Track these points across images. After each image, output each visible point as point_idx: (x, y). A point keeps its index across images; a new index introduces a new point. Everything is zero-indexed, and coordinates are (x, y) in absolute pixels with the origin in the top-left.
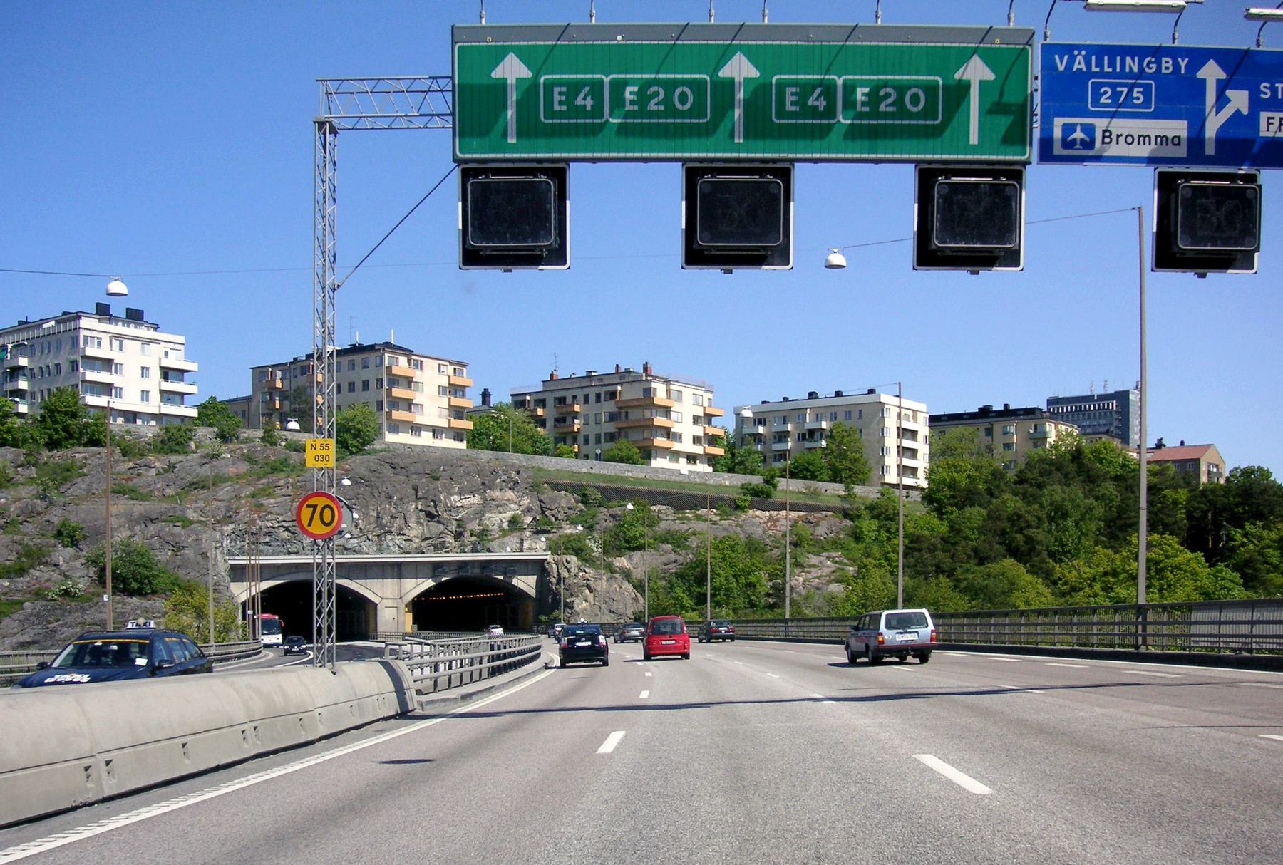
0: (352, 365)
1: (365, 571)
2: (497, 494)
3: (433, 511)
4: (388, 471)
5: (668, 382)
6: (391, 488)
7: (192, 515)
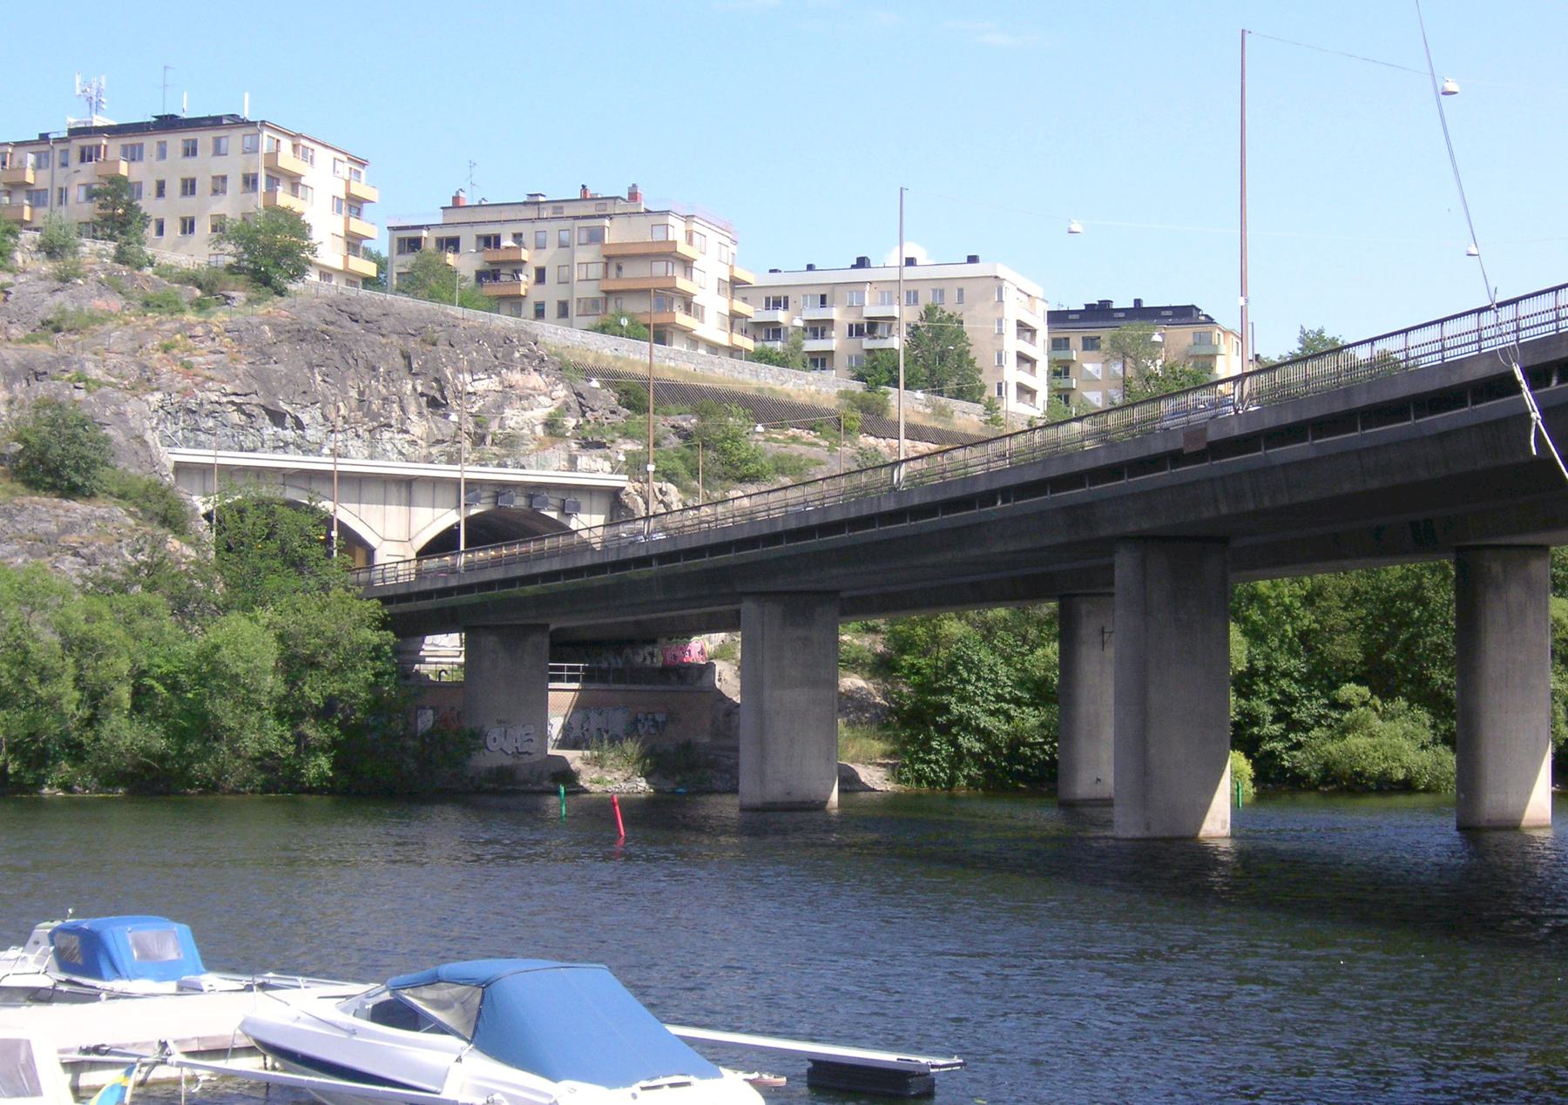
0: (191, 150)
1: (358, 484)
2: (515, 377)
3: (438, 396)
5: (688, 218)
7: (95, 373)
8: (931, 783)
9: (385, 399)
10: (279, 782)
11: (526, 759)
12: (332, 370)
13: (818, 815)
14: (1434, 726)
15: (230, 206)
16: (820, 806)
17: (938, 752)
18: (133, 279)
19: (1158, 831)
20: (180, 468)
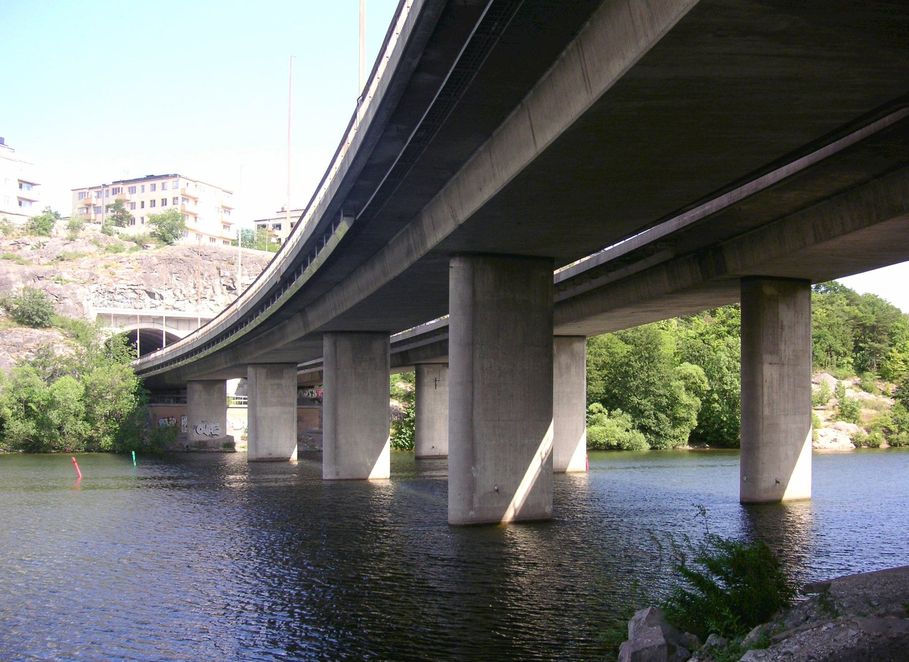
0: (154, 188)
4: (196, 256)
6: (201, 268)
7: (66, 276)
8: (401, 447)
9: (205, 288)
10: (91, 446)
11: (216, 437)
12: (182, 275)
13: (284, 465)
14: (633, 421)
15: (159, 211)
16: (287, 460)
17: (405, 434)
18: (105, 239)
19: (343, 475)
20: (100, 316)
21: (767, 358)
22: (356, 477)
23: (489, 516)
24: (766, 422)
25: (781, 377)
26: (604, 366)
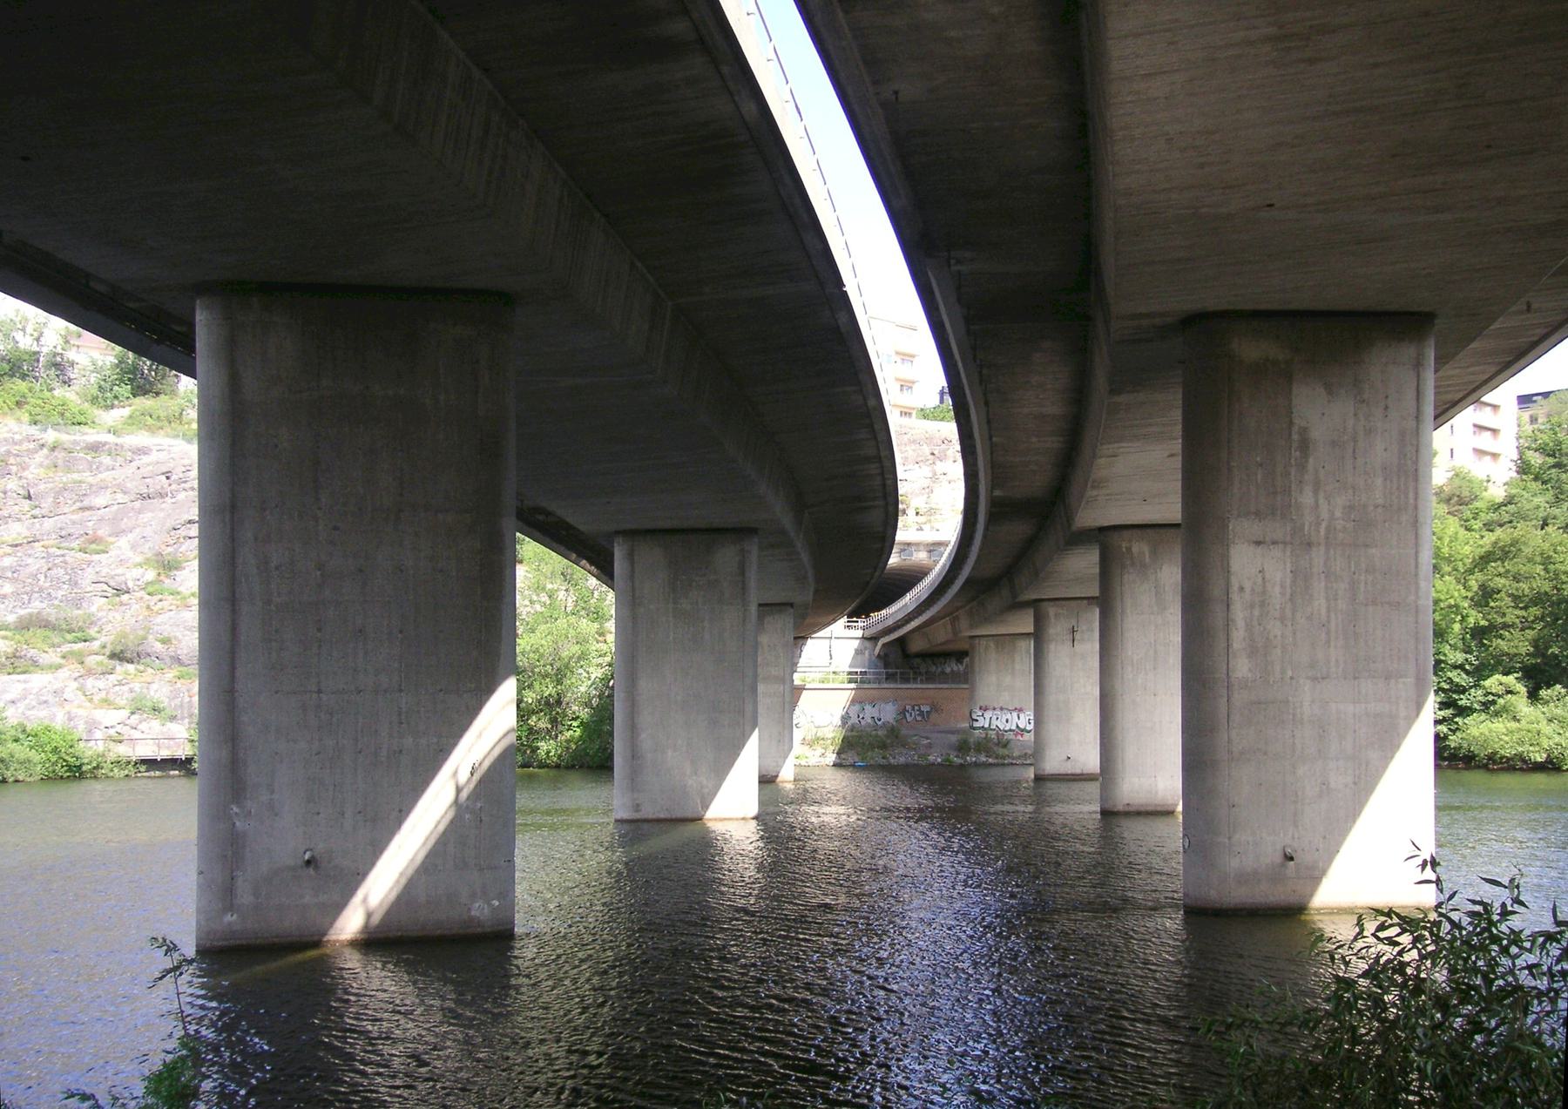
21: (1242, 527)
22: (678, 814)
23: (287, 924)
24: (1239, 698)
25: (1301, 577)
26: (1538, 599)
